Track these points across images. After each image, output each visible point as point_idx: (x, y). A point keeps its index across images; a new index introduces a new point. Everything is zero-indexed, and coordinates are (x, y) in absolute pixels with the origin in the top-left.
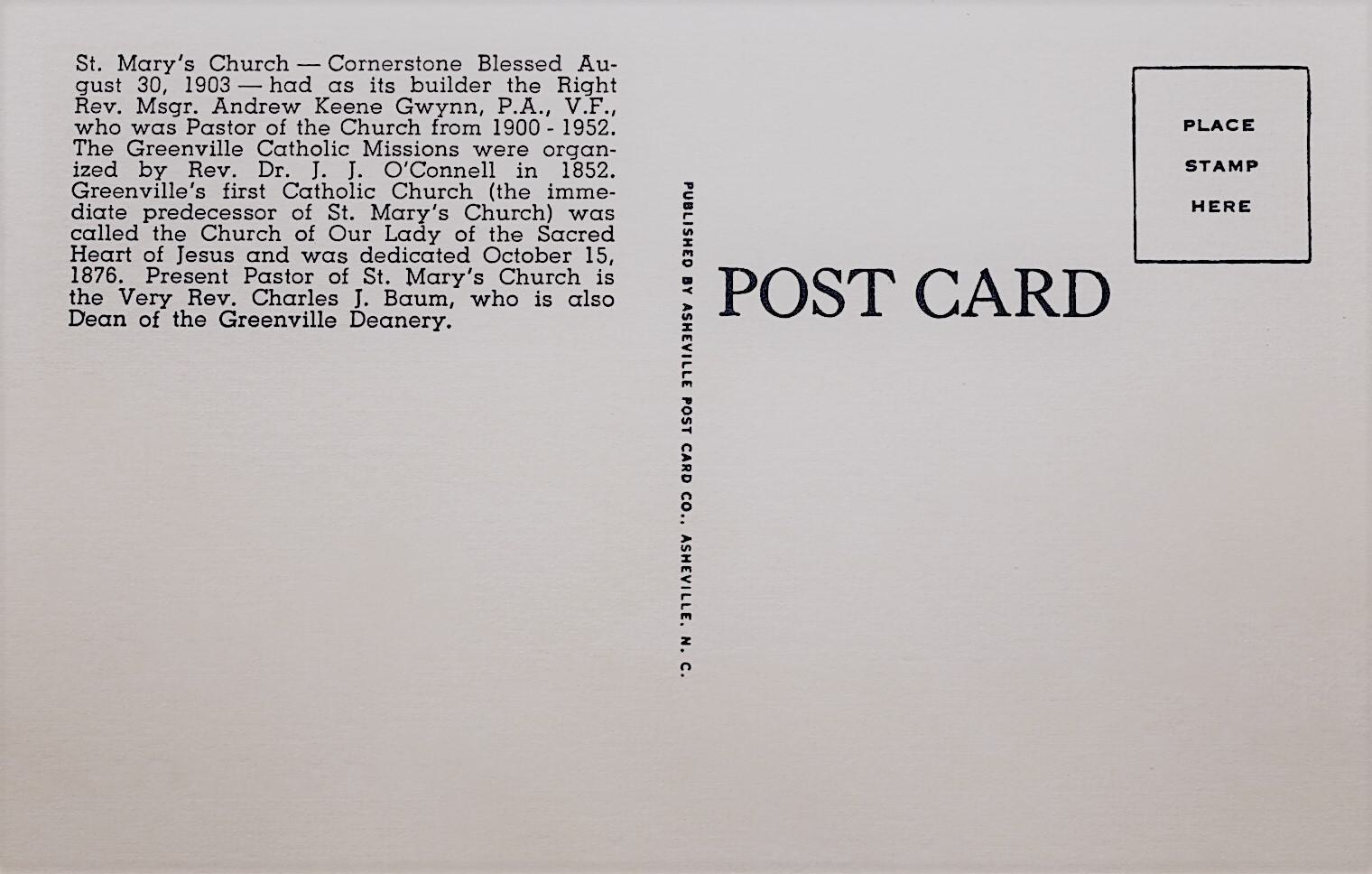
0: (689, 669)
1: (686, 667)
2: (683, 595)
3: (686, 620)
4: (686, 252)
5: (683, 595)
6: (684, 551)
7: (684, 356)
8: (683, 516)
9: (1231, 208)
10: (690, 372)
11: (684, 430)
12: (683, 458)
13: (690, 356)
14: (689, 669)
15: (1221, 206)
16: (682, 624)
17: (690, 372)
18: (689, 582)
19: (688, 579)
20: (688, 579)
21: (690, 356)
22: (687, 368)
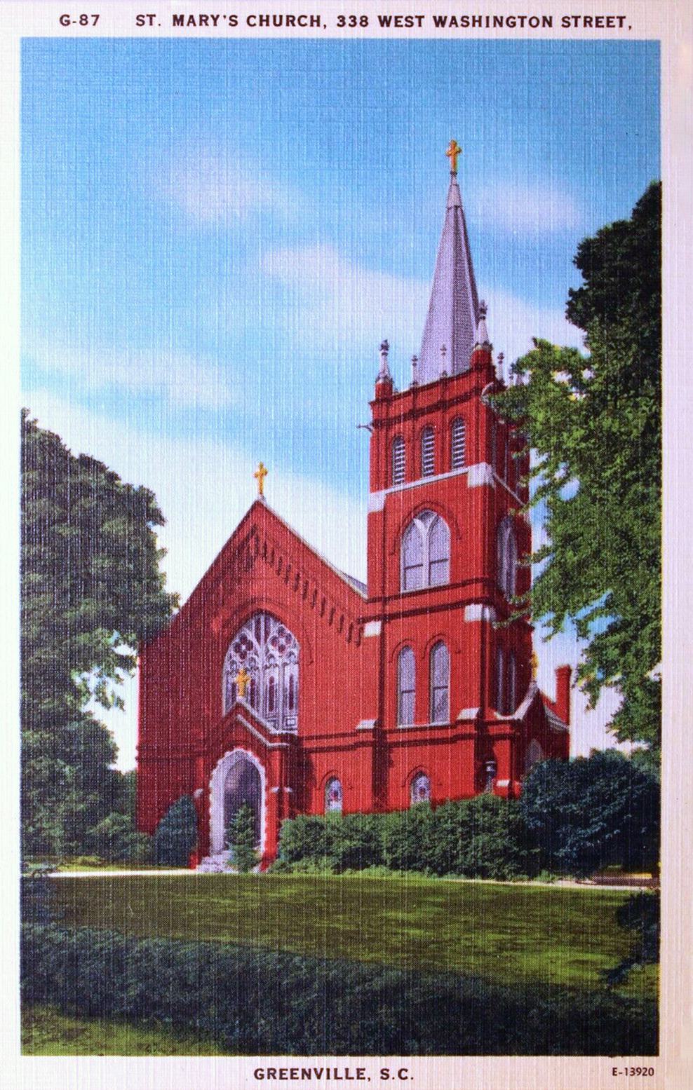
0: (406, 1070)
1: (404, 1074)
2: (336, 1078)
3: (366, 1074)
4: (353, 18)
5: (336, 1078)
6: (468, 23)
7: (328, 1078)
8: (225, 17)
9: (273, 1075)
10: (347, 1070)
11: (420, 25)
12: (191, 25)
13: (328, 1070)
14: (406, 1070)
15: (299, 1074)
16: (369, 1079)
17: (347, 1070)
18: (322, 1070)
19: (319, 1072)
20: (319, 1072)
21: (328, 1070)
22: (341, 1073)
